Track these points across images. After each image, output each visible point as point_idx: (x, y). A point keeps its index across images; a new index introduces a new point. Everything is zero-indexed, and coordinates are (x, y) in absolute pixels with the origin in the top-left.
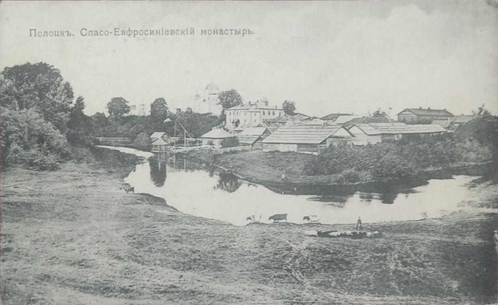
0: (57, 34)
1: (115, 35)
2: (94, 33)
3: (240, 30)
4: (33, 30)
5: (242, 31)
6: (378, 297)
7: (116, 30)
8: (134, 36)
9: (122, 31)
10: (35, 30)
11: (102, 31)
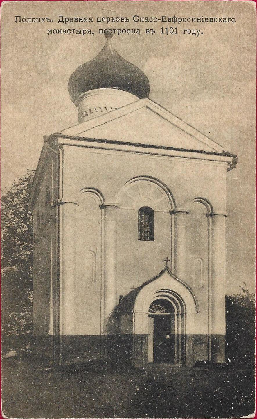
1: (163, 21)
10: (20, 17)
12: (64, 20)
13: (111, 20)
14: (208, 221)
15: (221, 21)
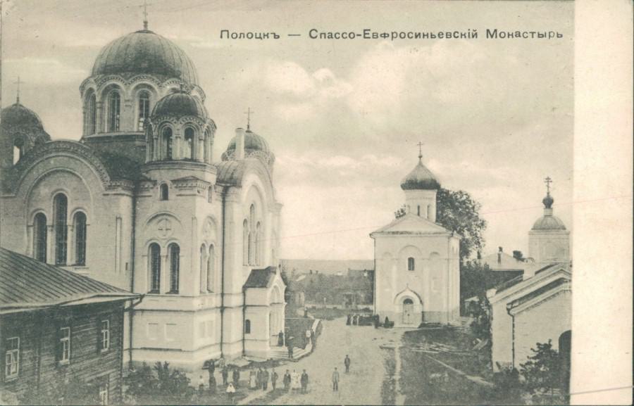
2: (327, 35)
6: (86, 373)
7: (366, 32)
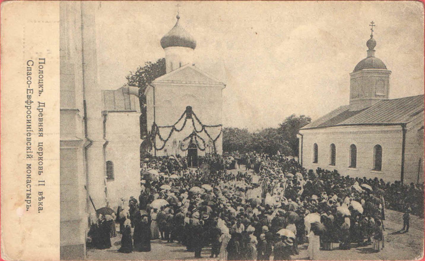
0: (40, 81)
1: (27, 90)
3: (30, 198)
4: (45, 61)
5: (29, 199)
8: (37, 153)
9: (31, 96)
10: (44, 63)
11: (31, 79)
12: (41, 108)
13: (40, 157)
14: (302, 163)
15: (39, 205)
